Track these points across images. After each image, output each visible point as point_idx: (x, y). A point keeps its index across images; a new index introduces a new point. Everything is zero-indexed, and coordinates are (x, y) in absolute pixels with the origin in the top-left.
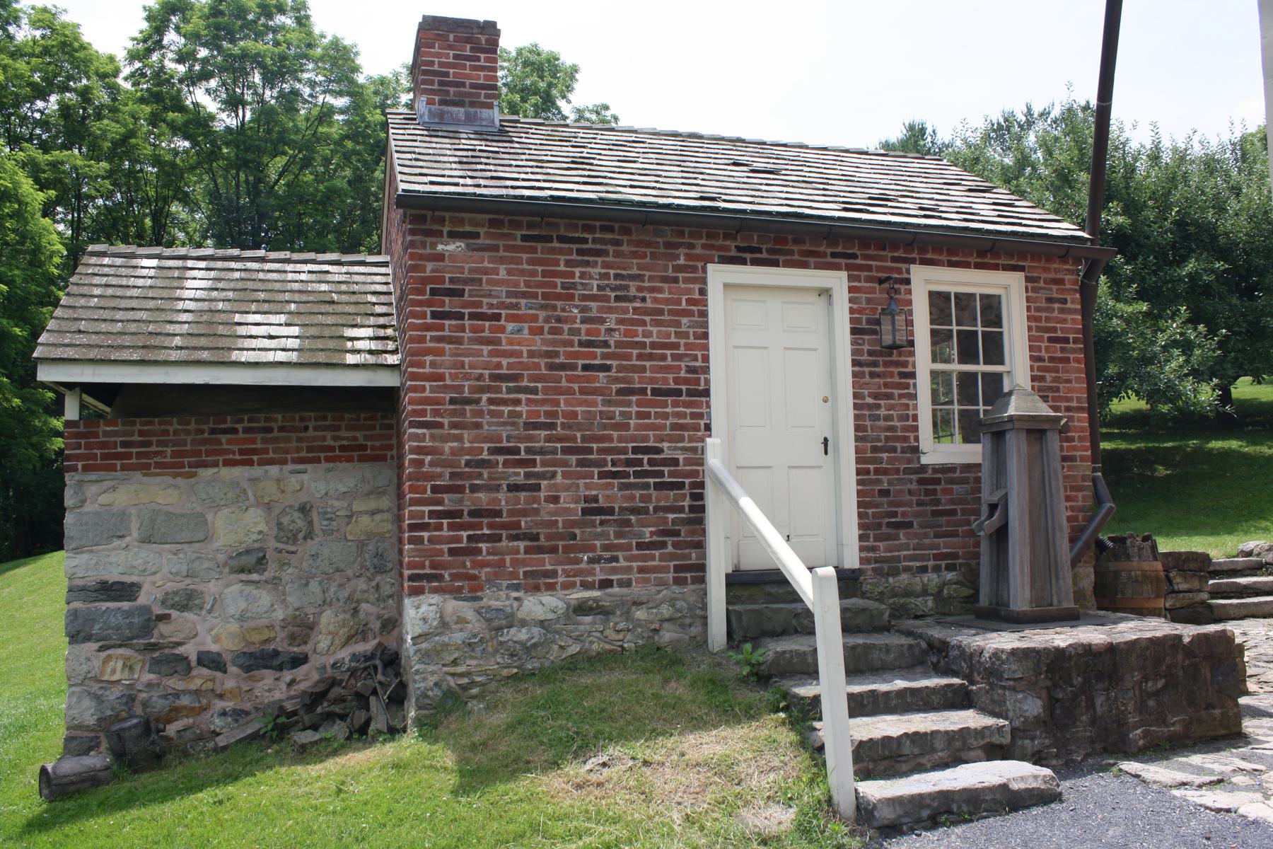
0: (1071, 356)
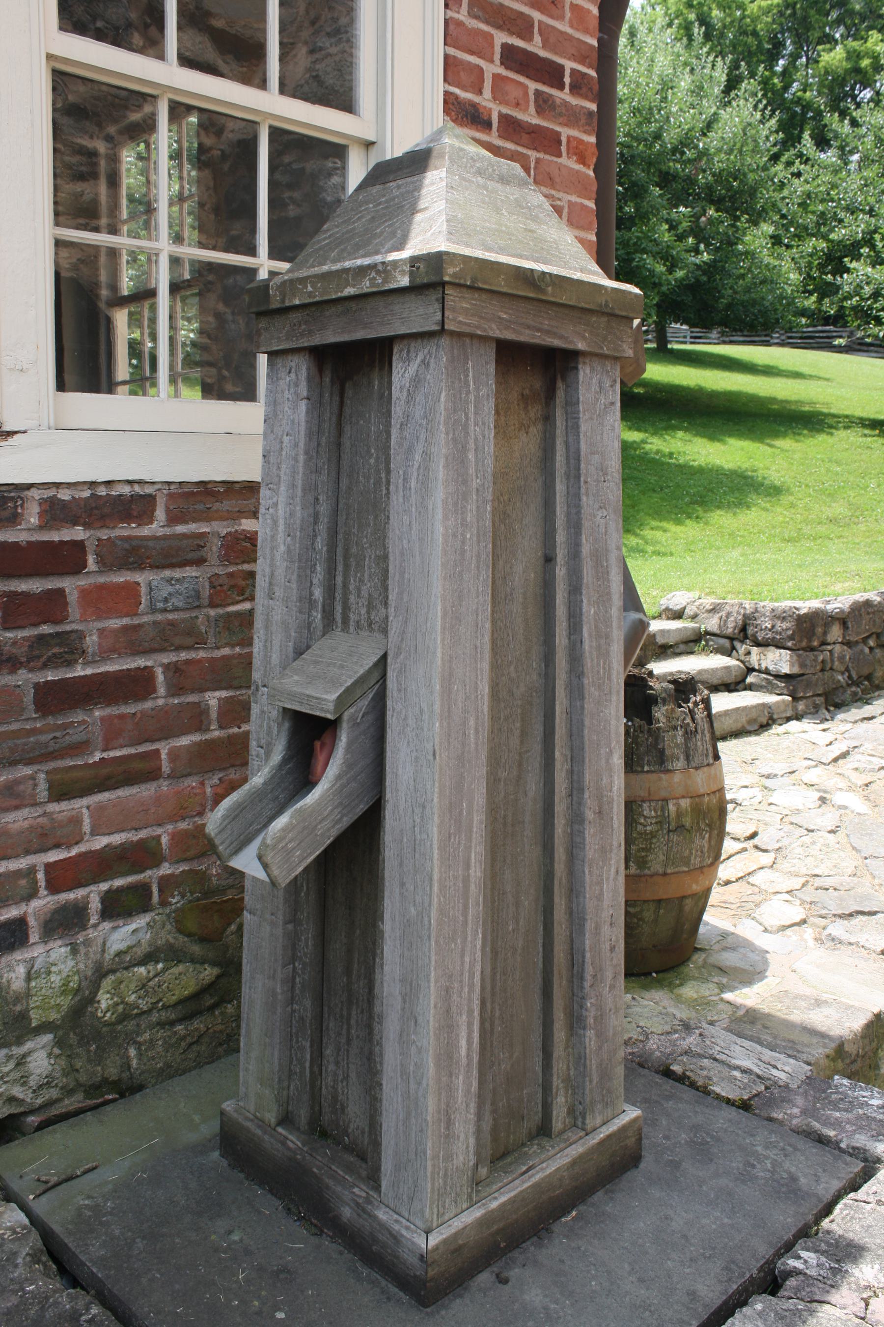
0: (565, 132)
